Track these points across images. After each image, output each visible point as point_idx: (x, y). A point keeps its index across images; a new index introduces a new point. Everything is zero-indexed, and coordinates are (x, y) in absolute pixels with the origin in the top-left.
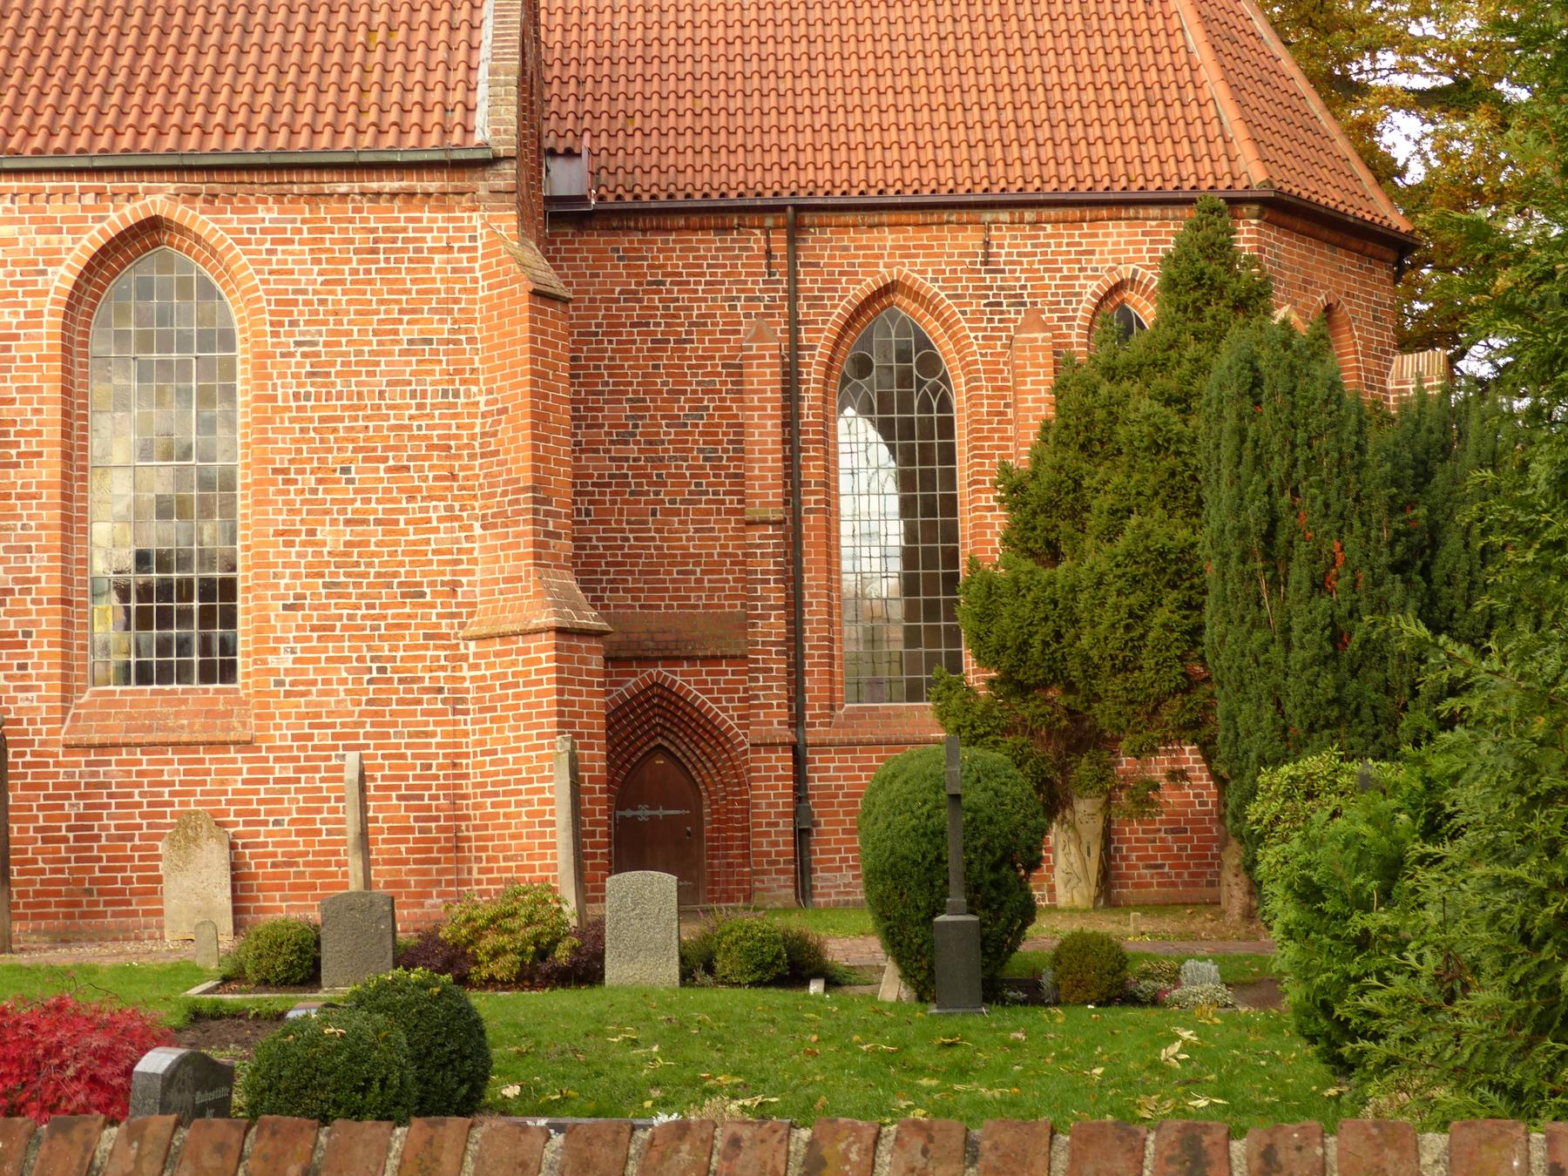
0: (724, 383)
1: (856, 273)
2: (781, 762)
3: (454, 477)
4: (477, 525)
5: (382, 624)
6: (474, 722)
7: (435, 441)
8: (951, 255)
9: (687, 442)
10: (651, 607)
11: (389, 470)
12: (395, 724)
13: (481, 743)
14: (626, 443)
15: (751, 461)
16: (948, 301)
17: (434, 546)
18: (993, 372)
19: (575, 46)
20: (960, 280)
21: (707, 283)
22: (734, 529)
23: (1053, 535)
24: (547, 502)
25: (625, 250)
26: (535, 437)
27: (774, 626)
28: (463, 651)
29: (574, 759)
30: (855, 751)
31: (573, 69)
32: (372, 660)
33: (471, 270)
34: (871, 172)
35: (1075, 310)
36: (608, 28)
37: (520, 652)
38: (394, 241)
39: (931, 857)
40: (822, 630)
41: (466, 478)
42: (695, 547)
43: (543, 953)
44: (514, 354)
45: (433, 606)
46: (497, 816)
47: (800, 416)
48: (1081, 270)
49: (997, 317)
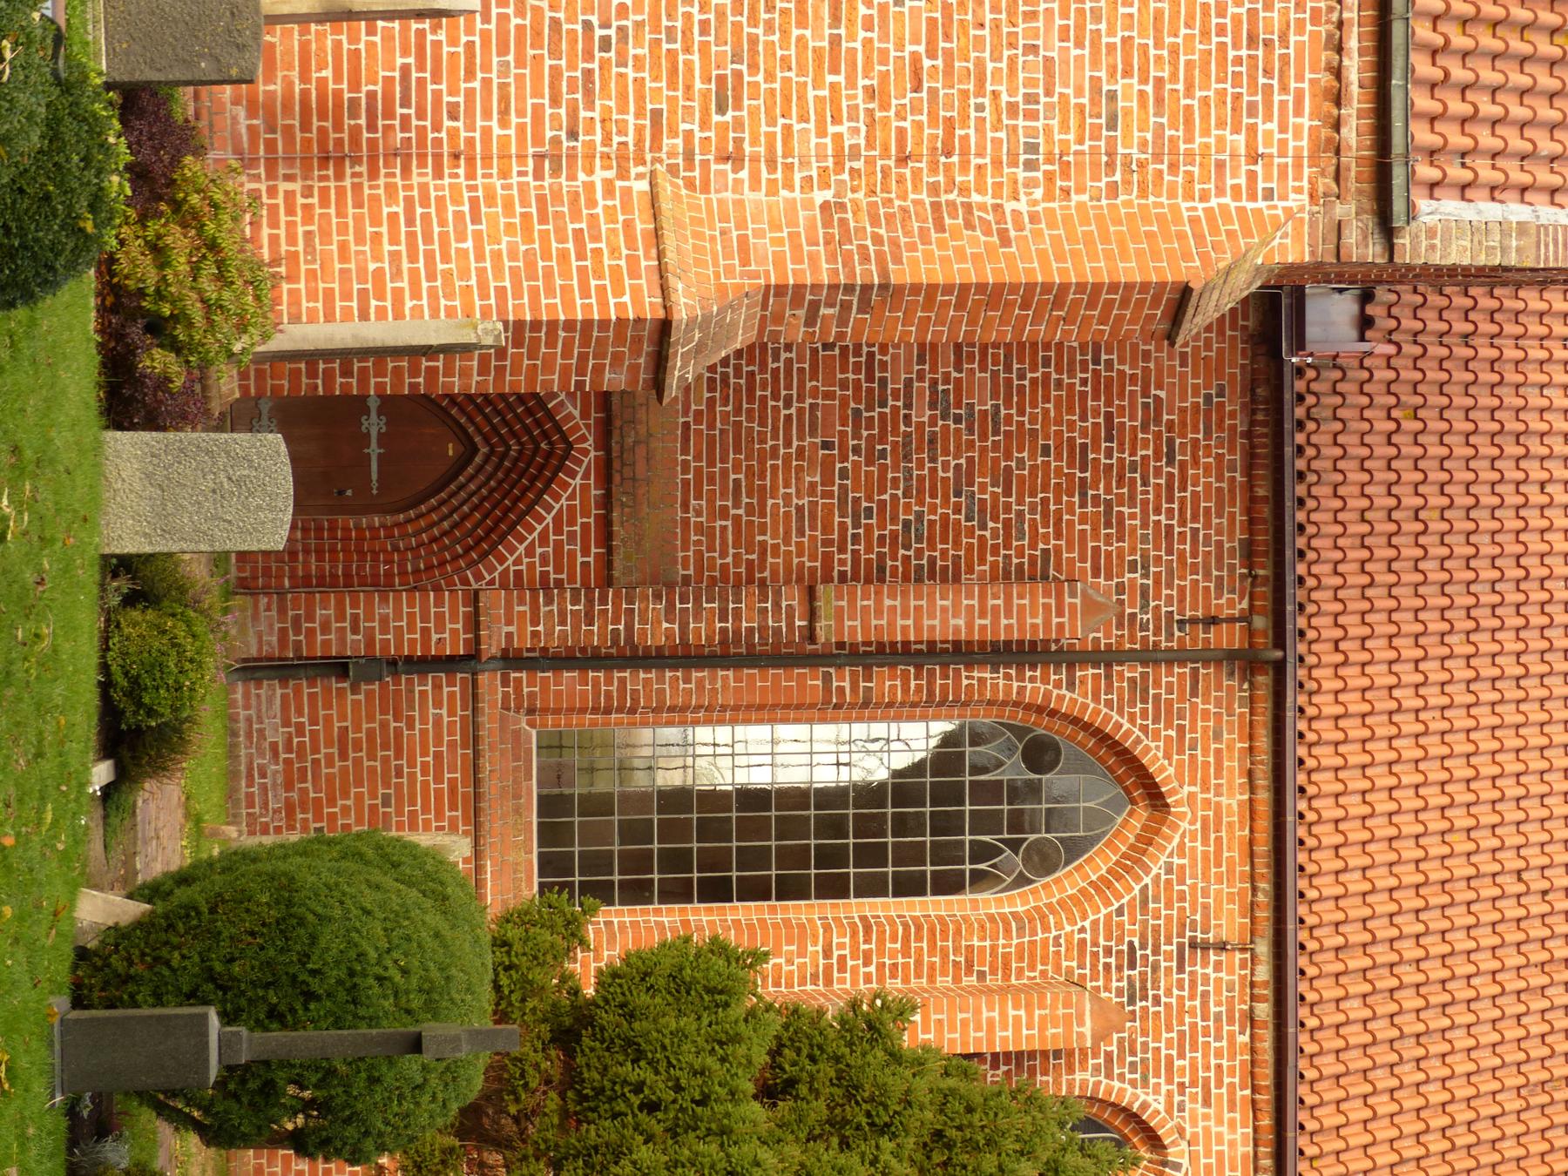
0: (1020, 554)
1: (1181, 752)
2: (450, 637)
3: (903, 160)
4: (828, 195)
5: (678, 46)
6: (523, 188)
7: (958, 132)
8: (1206, 894)
9: (933, 495)
10: (686, 439)
11: (916, 59)
12: (520, 63)
13: (490, 199)
14: (933, 406)
15: (905, 594)
16: (1137, 888)
17: (797, 127)
18: (1030, 954)
19: (1520, 330)
20: (1169, 906)
21: (1170, 528)
22: (801, 565)
23: (803, 1090)
24: (865, 306)
25: (1221, 405)
26: (965, 288)
27: (657, 629)
28: (634, 171)
29: (466, 349)
30: (464, 746)
31: (1487, 327)
32: (620, 29)
33: (1220, 192)
34: (1330, 775)
35: (1121, 1077)
36: (1544, 379)
37: (633, 261)
38: (1268, 73)
39: (315, 985)
40: (648, 698)
41: (901, 180)
42: (776, 506)
43: (157, 328)
44: (1093, 257)
45: (705, 125)
46: (376, 221)
47: (969, 667)
48: (1181, 1085)
49: (1113, 960)
